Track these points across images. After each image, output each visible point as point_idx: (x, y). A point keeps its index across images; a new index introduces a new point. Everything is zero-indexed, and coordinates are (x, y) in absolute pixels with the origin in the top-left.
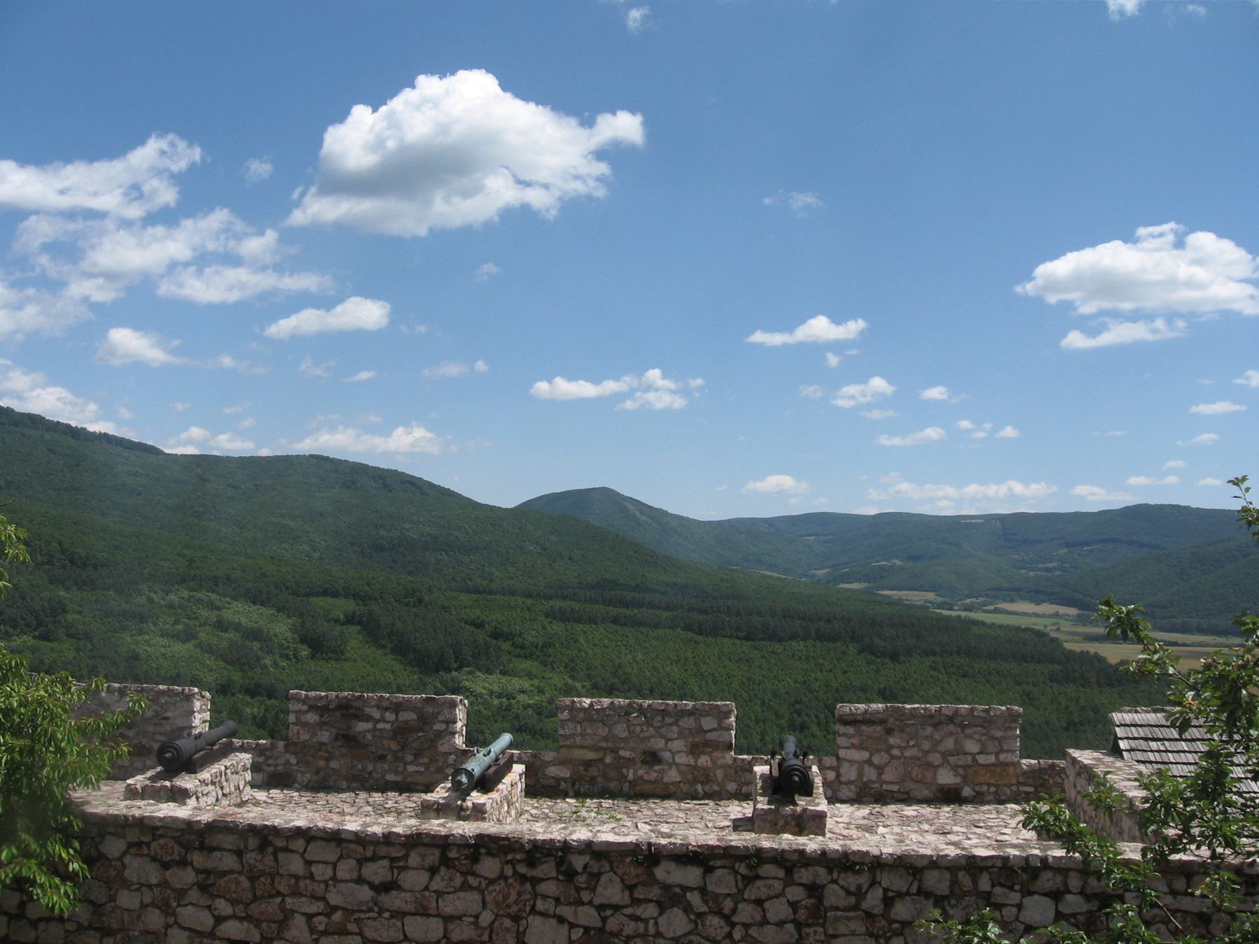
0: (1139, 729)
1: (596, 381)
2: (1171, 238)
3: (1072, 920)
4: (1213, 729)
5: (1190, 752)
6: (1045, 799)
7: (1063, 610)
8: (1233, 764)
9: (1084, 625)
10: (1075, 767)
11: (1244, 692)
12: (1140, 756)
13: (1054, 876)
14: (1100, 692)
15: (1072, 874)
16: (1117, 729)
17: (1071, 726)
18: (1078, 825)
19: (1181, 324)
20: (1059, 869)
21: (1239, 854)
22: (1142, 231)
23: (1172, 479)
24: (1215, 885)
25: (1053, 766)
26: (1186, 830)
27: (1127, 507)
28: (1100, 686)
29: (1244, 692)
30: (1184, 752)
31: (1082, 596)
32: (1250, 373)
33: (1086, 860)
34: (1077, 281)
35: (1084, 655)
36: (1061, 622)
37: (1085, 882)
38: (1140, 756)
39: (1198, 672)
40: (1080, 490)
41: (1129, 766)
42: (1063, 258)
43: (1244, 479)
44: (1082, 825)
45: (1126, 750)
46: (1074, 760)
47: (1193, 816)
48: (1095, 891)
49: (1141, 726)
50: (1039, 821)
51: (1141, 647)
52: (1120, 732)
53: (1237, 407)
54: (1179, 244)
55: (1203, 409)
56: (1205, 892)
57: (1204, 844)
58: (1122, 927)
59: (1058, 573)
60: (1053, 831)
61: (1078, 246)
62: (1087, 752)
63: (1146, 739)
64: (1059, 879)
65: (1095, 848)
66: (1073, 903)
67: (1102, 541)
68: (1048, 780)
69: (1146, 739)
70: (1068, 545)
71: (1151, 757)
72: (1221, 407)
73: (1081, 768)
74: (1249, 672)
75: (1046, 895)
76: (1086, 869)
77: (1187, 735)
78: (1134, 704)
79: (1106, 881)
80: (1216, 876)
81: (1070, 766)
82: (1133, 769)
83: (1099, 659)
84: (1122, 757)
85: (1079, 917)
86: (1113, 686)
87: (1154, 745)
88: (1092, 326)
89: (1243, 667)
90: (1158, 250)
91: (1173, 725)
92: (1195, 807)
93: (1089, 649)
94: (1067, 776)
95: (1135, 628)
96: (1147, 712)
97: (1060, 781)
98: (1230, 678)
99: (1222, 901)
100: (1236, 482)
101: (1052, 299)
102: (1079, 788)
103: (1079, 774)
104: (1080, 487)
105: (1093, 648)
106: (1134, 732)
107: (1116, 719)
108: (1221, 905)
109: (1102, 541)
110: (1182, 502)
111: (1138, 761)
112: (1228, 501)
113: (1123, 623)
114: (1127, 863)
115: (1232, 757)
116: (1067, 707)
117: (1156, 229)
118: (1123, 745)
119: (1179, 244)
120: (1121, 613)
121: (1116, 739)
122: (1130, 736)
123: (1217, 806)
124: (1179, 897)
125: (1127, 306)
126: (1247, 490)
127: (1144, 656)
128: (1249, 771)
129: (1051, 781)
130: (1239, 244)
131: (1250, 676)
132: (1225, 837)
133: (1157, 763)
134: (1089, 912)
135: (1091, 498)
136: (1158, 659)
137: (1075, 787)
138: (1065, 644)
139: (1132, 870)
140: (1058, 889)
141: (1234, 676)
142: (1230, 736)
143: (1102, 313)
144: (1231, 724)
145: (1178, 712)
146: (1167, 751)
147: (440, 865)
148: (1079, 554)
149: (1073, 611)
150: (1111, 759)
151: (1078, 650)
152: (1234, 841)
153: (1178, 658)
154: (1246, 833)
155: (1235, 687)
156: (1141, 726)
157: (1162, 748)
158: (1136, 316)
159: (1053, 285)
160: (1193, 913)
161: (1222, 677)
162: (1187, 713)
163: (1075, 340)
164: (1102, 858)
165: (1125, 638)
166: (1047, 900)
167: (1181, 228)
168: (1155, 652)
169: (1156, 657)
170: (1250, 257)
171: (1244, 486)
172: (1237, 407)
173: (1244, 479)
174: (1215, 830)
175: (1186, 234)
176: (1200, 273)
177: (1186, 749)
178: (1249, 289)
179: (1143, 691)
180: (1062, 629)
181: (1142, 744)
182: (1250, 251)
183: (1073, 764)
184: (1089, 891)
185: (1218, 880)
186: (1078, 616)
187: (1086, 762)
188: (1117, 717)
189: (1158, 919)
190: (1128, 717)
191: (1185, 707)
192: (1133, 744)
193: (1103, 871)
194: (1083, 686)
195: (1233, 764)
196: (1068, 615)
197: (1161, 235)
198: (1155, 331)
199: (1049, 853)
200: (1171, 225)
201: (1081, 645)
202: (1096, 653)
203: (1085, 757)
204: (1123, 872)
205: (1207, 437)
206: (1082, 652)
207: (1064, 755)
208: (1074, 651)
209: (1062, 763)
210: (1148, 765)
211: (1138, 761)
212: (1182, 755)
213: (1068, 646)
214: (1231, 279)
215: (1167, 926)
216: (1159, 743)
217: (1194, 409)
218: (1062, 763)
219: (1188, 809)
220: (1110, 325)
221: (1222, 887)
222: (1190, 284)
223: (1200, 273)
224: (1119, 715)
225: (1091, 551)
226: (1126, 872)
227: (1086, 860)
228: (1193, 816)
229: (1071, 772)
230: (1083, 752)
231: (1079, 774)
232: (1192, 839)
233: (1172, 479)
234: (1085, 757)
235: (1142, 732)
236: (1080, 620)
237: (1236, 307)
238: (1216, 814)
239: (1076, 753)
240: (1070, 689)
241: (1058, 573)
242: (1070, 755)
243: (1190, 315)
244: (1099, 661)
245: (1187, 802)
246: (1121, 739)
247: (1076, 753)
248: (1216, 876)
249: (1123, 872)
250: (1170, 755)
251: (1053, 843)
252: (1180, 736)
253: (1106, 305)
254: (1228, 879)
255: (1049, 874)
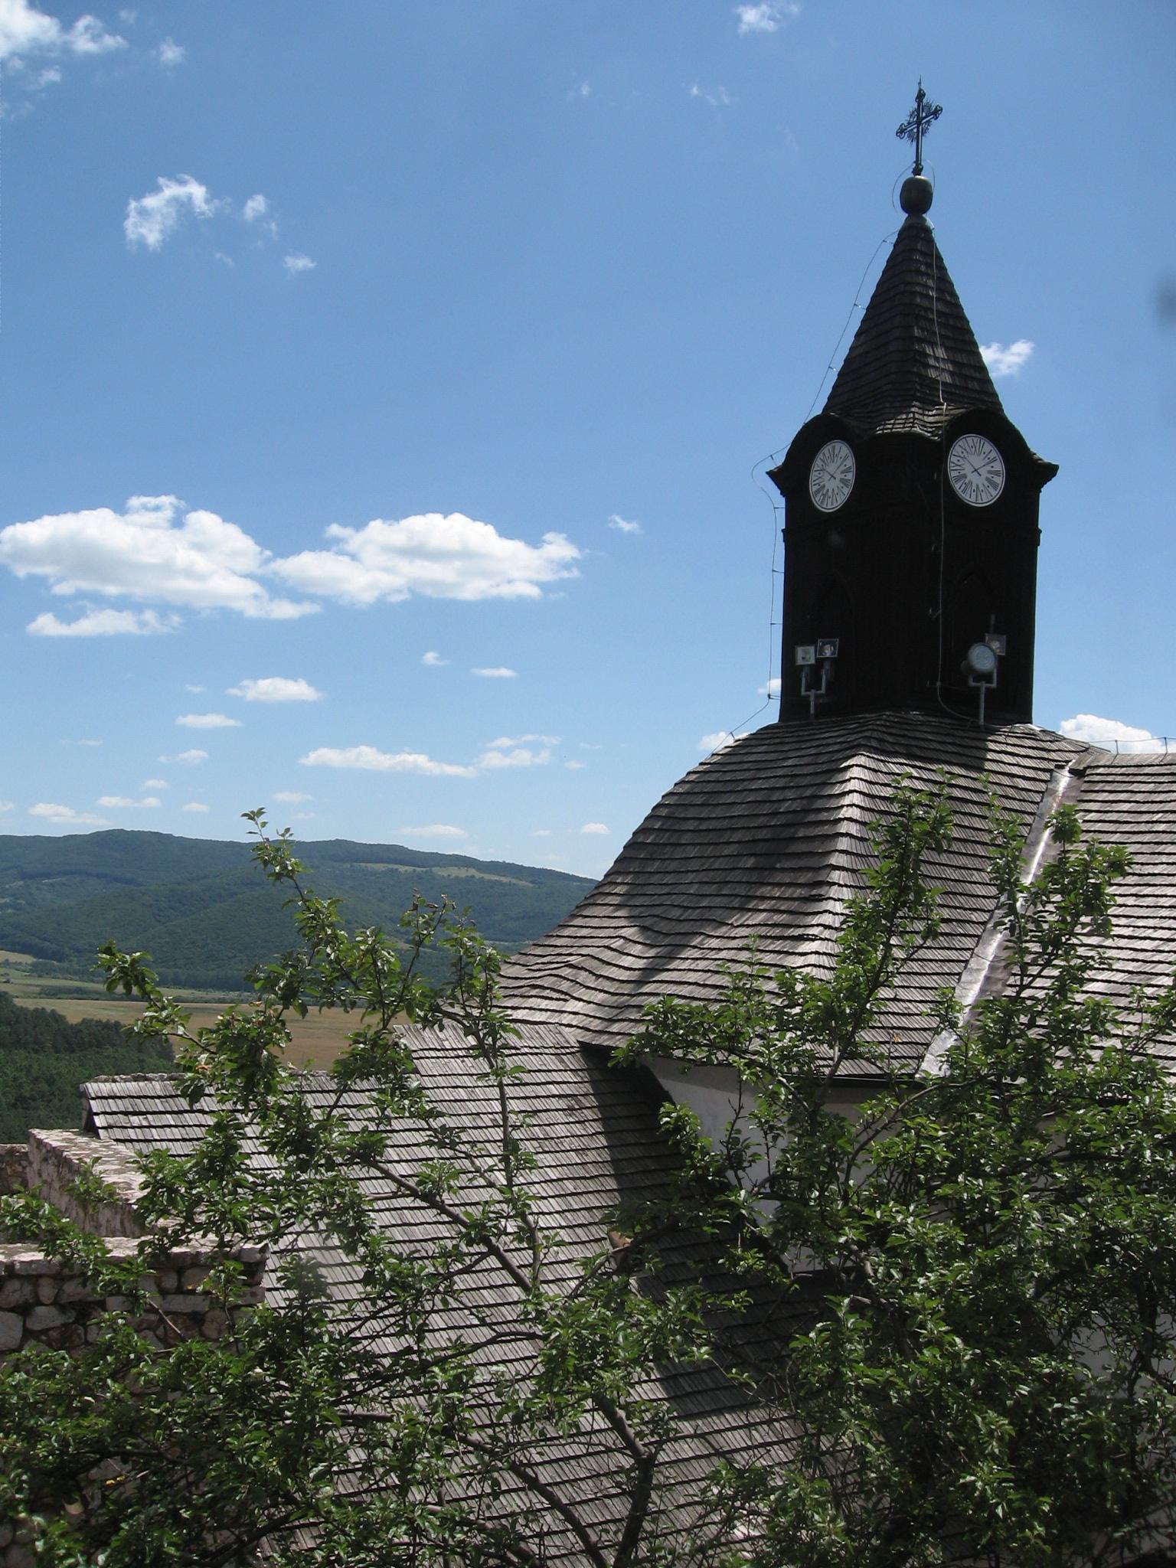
0: (119, 1101)
1: (385, 749)
2: (169, 513)
3: (44, 1338)
4: (226, 1098)
5: (176, 1126)
6: (19, 1192)
7: (15, 957)
8: (245, 1137)
9: (40, 976)
10: (40, 1151)
11: (265, 1053)
12: (119, 1134)
13: (22, 1285)
14: (57, 1059)
15: (44, 1282)
16: (92, 1102)
17: (21, 1103)
18: (59, 1221)
19: (176, 619)
20: (30, 1276)
21: (250, 1239)
22: (135, 502)
23: (152, 802)
24: (220, 1277)
25: (12, 1151)
26: (189, 1218)
27: (98, 834)
28: (57, 1052)
29: (265, 1053)
30: (170, 1126)
31: (37, 940)
32: (246, 682)
33: (67, 1262)
34: (53, 552)
35: (40, 1013)
36: (13, 973)
37: (60, 1290)
38: (119, 1134)
39: (212, 1032)
40: (42, 809)
41: (105, 1147)
42: (38, 521)
43: (260, 812)
44: (64, 1220)
45: (103, 1128)
46: (40, 1143)
47: (199, 1200)
48: (71, 1300)
49: (121, 1098)
50: (12, 1219)
51: (147, 1004)
52: (95, 1106)
53: (231, 723)
54: (178, 523)
55: (192, 720)
56: (207, 1288)
57: (211, 1231)
58: (111, 1338)
59: (10, 911)
60: (29, 1230)
61: (57, 509)
62: (56, 1132)
63: (126, 1113)
64: (28, 1289)
65: (80, 1247)
66: (46, 1316)
67: (66, 873)
68: (5, 1169)
69: (126, 1113)
70: (24, 876)
71: (132, 1134)
72: (214, 720)
73: (48, 1151)
74: (270, 1029)
75: (11, 1310)
76: (66, 1272)
77: (197, 1106)
78: (115, 1070)
79: (92, 1286)
80: (221, 1268)
81: (35, 1151)
82: (111, 1150)
83: (57, 1018)
84: (98, 1136)
85: (51, 1332)
86: (73, 1051)
87: (135, 1120)
88: (69, 609)
89: (262, 1024)
90: (152, 526)
91: (184, 1095)
92: (201, 1189)
93: (46, 1006)
94: (31, 1163)
95: (140, 981)
96: (126, 1081)
97: (20, 1169)
98: (250, 1038)
99: (226, 1296)
100: (252, 816)
101: (21, 571)
102: (45, 1176)
103: (45, 1160)
104: (41, 805)
105: (49, 1005)
106: (113, 1105)
107: (90, 1091)
108: (225, 1301)
109: (66, 873)
110: (164, 830)
111: (117, 1140)
112: (241, 833)
113: (126, 974)
114: (117, 1262)
115: (242, 1129)
116: (15, 1079)
117: (152, 501)
118: (99, 1121)
119: (178, 523)
120: (125, 962)
121: (92, 1114)
122: (108, 1110)
123: (227, 1184)
124: (169, 1297)
125: (112, 590)
126: (264, 824)
127: (151, 1014)
128: (265, 1144)
129: (9, 1170)
130: (246, 530)
131: (271, 1034)
132: (234, 1220)
133: (138, 1141)
134: (64, 1325)
135: (55, 819)
136: (166, 1018)
137: (40, 1176)
138: (15, 1000)
139: (124, 1269)
140: (26, 1302)
141: (254, 1034)
142: (246, 1104)
143: (81, 595)
144: (249, 1087)
145: (190, 1079)
146: (150, 1127)
147: (245, 1264)
148: (38, 889)
149: (27, 959)
150: (85, 1139)
151: (32, 1008)
152: (244, 1225)
153: (188, 1017)
154: (256, 1215)
155: (255, 1048)
156: (121, 1098)
157: (145, 1123)
158: (121, 604)
159: (22, 554)
160: (185, 1314)
161: (241, 1036)
162: (200, 1079)
163: (47, 625)
164: (87, 1256)
165: (128, 996)
166: (13, 1315)
167: (183, 504)
168: (164, 1008)
169: (164, 1014)
170: (258, 549)
171: (261, 819)
172: (231, 723)
173: (260, 812)
174: (223, 1214)
175: (188, 512)
176: (200, 562)
177: (173, 1123)
178: (253, 588)
179: (108, 1057)
180: (12, 980)
181: (122, 1120)
182: (258, 543)
183: (38, 1147)
184: (64, 1300)
185: (222, 1271)
186: (34, 965)
187: (55, 1144)
188: (93, 1088)
189: (144, 1326)
190: (105, 1088)
191: (197, 1072)
192: (111, 1119)
193: (90, 1273)
194: (36, 1052)
195: (245, 1137)
196: (20, 963)
197: (157, 508)
198: (143, 624)
199: (16, 1258)
200: (166, 500)
201: (35, 1000)
202: (53, 1011)
203: (53, 1138)
204: (112, 1273)
205: (195, 755)
206: (36, 1010)
207: (27, 1138)
208: (26, 1009)
209: (24, 1148)
210: (129, 1144)
211: (117, 1140)
212: (168, 1130)
213: (19, 1002)
214: (235, 573)
215: (155, 1332)
216: (141, 1117)
217: (181, 721)
218: (24, 1148)
219: (194, 1192)
220: (88, 612)
221: (228, 1281)
222: (189, 573)
223: (200, 562)
224: (95, 1085)
225: (52, 885)
226: (117, 1272)
227: (67, 1262)
228: (199, 1200)
229: (36, 1158)
230: (50, 1132)
231: (45, 1160)
232: (199, 1227)
233: (152, 802)
234: (53, 1138)
235: (121, 1105)
236: (36, 971)
237: (237, 605)
238: (224, 1195)
239: (42, 1134)
240: (20, 1056)
241: (10, 911)
242: (34, 1136)
243: (186, 610)
244: (57, 1021)
245: (191, 1185)
246: (97, 1114)
247: (42, 1134)
248: (221, 1268)
249: (112, 1273)
250: (153, 1130)
251: (19, 1245)
252: (191, 1105)
253: (85, 585)
254: (234, 1269)
255: (16, 1284)
